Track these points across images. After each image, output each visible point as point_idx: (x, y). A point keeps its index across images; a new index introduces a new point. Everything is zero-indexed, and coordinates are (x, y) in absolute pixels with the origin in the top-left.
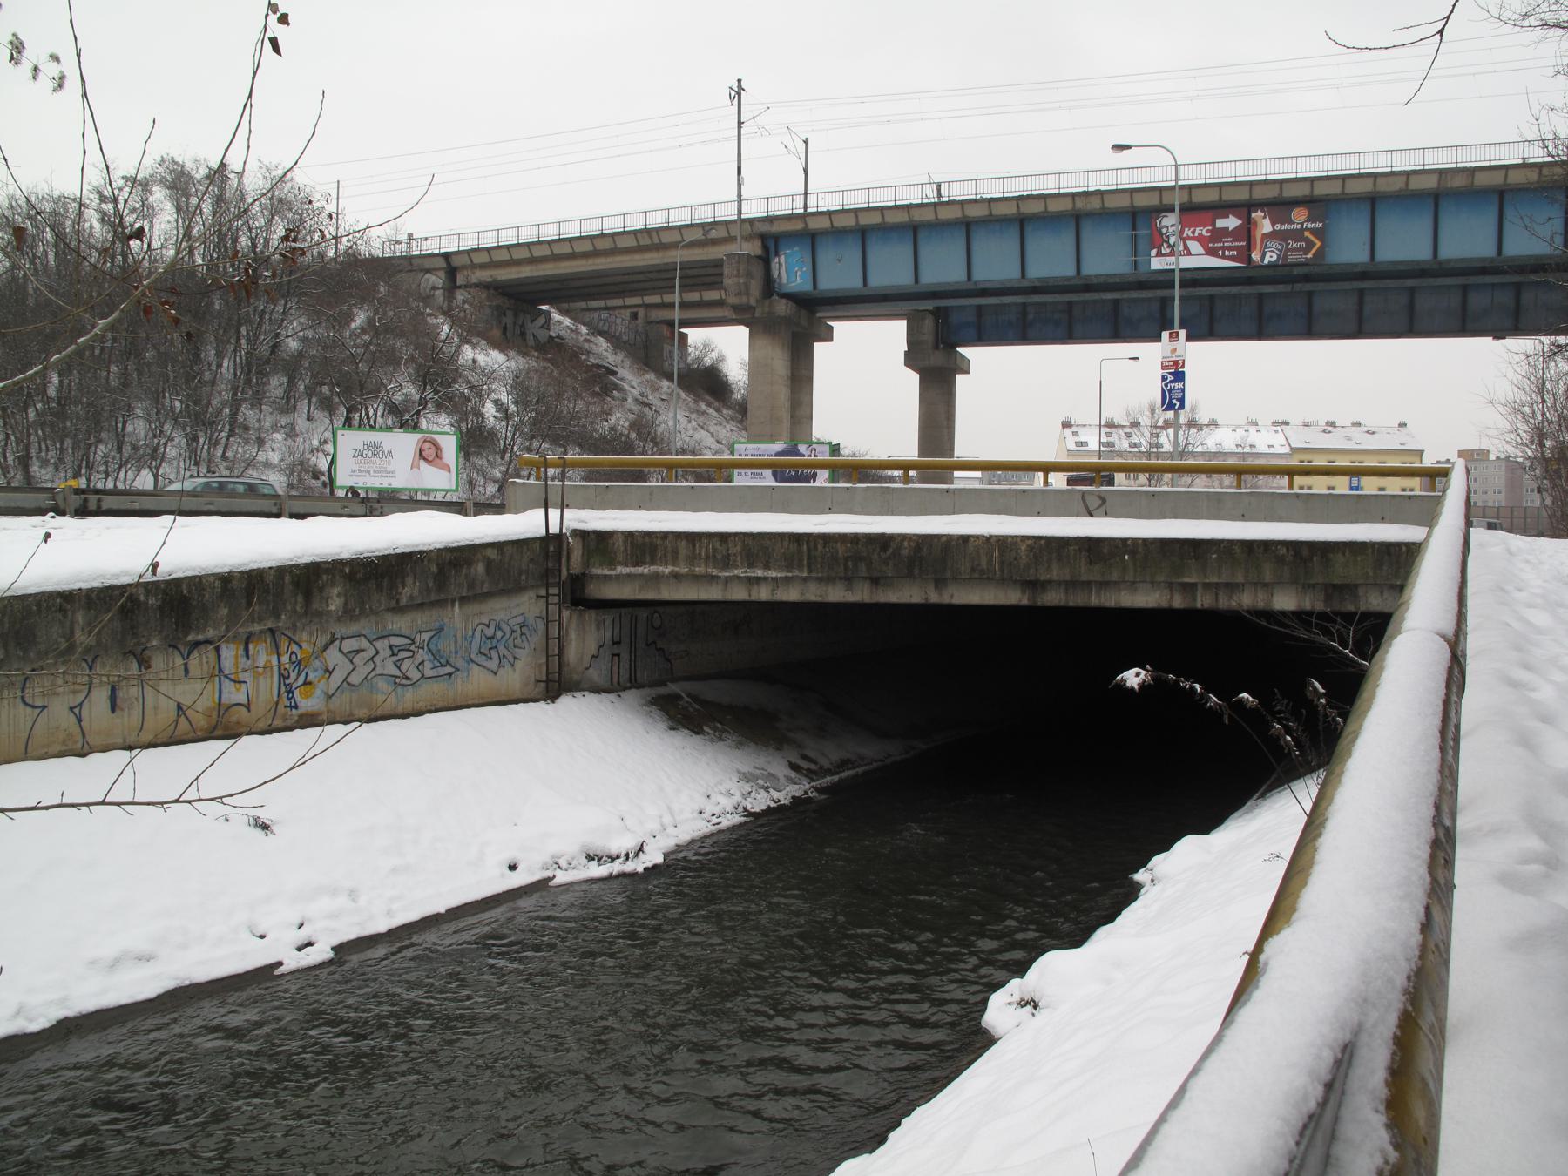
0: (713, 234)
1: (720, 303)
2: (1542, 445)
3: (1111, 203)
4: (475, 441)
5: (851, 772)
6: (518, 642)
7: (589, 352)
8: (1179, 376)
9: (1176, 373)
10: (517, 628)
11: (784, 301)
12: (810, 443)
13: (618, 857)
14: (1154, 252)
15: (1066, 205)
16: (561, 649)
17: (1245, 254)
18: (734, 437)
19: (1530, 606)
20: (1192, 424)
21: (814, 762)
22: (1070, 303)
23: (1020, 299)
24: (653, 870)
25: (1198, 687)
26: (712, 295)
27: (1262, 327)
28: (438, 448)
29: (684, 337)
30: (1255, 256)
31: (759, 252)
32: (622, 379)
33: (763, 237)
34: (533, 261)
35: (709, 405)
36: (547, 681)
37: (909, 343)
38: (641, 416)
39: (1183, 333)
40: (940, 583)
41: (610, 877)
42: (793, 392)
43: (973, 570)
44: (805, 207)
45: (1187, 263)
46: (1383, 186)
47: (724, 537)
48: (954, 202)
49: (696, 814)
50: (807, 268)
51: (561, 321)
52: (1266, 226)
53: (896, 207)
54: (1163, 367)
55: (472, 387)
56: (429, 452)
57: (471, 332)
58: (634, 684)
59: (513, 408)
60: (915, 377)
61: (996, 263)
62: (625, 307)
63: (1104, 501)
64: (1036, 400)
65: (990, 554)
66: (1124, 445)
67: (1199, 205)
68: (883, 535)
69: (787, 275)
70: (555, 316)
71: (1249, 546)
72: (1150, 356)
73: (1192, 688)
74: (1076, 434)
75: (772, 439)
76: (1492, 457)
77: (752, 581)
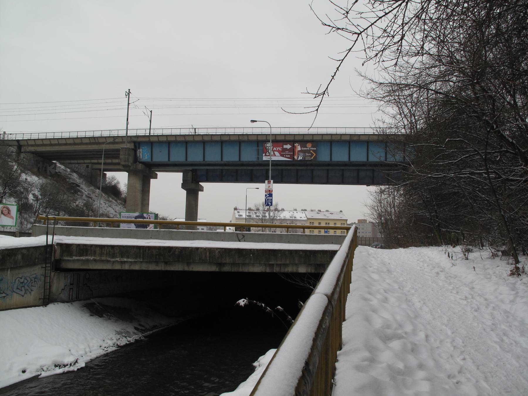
0: (117, 140)
1: (118, 164)
2: (381, 219)
3: (251, 138)
4: (24, 208)
5: (157, 330)
6: (33, 284)
7: (70, 178)
8: (271, 195)
9: (269, 194)
10: (33, 279)
11: (141, 164)
12: (148, 213)
13: (67, 365)
14: (264, 155)
15: (236, 138)
16: (50, 287)
17: (292, 157)
18: (121, 210)
19: (373, 272)
20: (276, 210)
21: (144, 327)
22: (237, 169)
23: (221, 168)
24: (80, 370)
25: (263, 305)
26: (116, 161)
27: (298, 179)
28: (9, 210)
29: (106, 174)
30: (296, 157)
31: (133, 147)
32: (82, 188)
33: (135, 143)
34: (51, 145)
35: (113, 199)
36: (44, 299)
37: (183, 180)
38: (88, 202)
39: (272, 181)
40: (188, 264)
41: (64, 373)
42: (143, 195)
43: (200, 259)
44: (150, 133)
45: (274, 158)
46: (334, 138)
47: (113, 247)
48: (200, 135)
49: (99, 347)
50: (149, 154)
51: (60, 167)
52: (299, 148)
53: (180, 135)
54: (266, 192)
55: (24, 189)
56: (6, 212)
57: (25, 169)
58: (78, 299)
59: (40, 197)
60: (185, 192)
61: (213, 155)
62: (84, 163)
63: (244, 236)
64: (225, 201)
65: (206, 253)
66: (254, 216)
67: (279, 140)
68: (169, 247)
69: (144, 155)
70: (58, 165)
71: (291, 252)
72: (262, 187)
73: (262, 305)
74: (238, 212)
75: (134, 211)
76: (368, 222)
77: (122, 263)
